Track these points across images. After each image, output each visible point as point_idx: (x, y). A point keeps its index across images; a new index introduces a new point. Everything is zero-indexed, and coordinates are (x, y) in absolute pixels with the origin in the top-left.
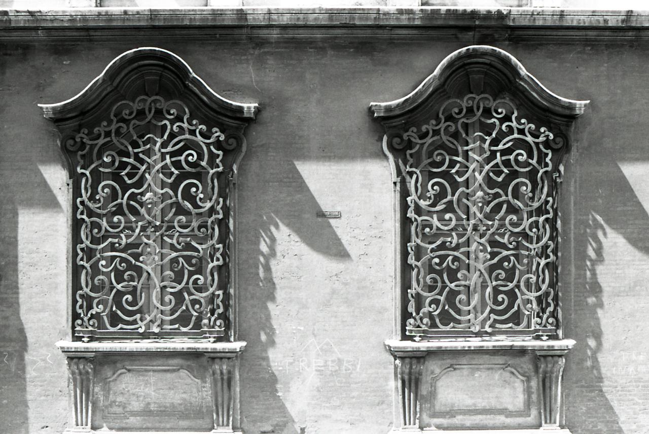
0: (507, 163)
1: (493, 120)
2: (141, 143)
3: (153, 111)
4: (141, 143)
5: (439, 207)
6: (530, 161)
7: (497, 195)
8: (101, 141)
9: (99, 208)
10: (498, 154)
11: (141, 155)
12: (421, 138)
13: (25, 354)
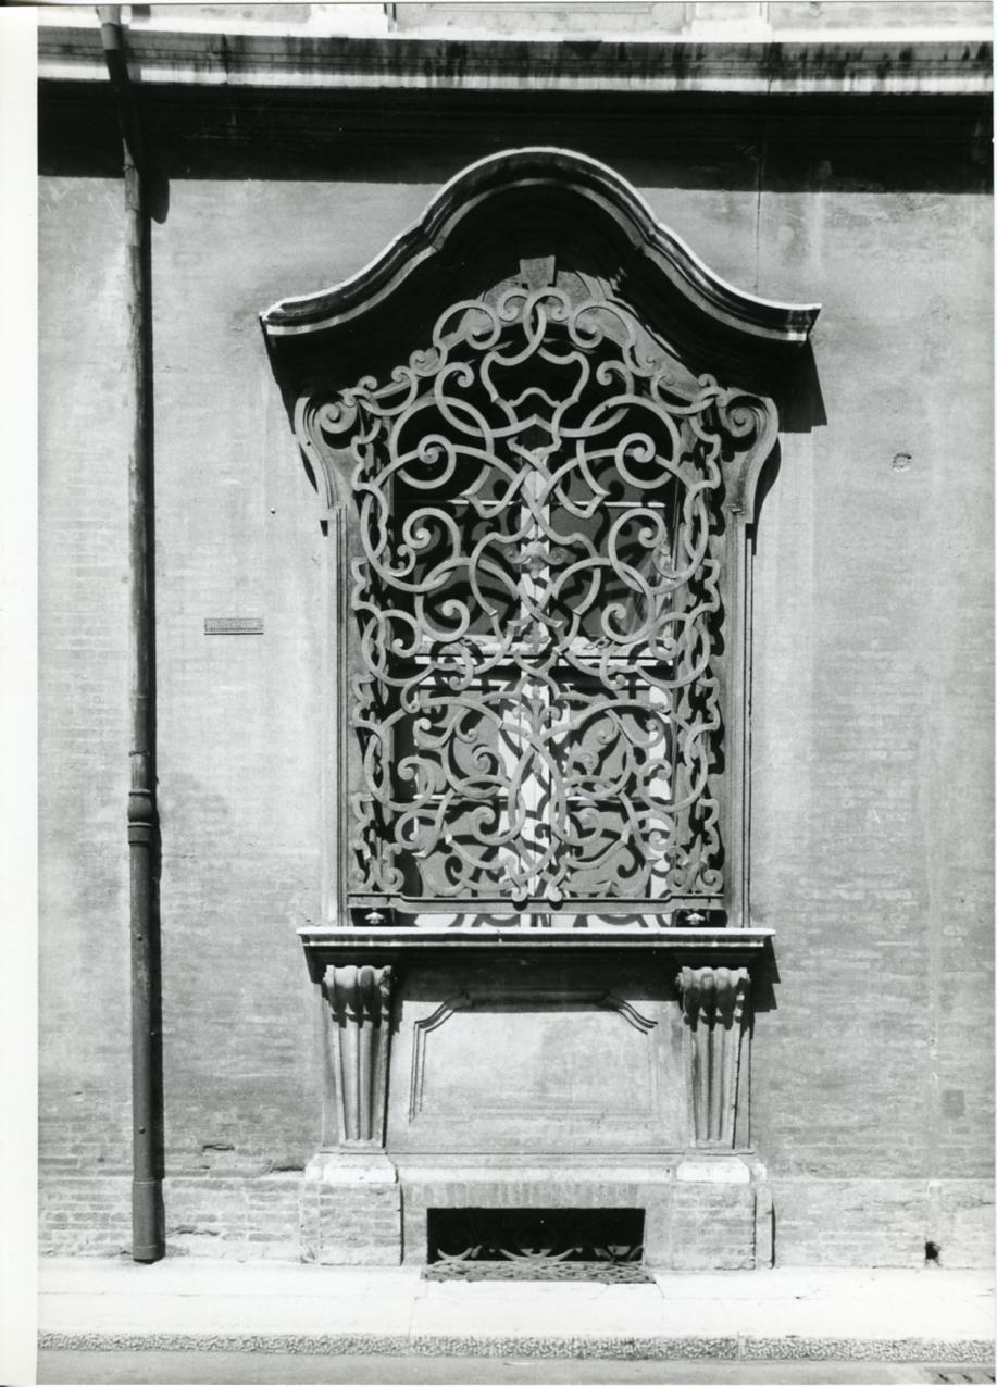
0: (597, 469)
1: (574, 356)
2: (511, 415)
3: (542, 328)
4: (511, 415)
5: (434, 581)
6: (662, 461)
7: (581, 553)
8: (408, 409)
9: (409, 579)
10: (580, 446)
11: (512, 446)
12: (386, 403)
13: (775, 985)
